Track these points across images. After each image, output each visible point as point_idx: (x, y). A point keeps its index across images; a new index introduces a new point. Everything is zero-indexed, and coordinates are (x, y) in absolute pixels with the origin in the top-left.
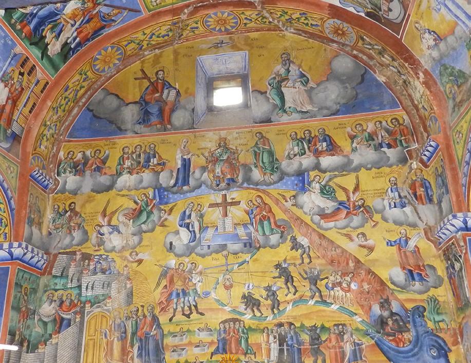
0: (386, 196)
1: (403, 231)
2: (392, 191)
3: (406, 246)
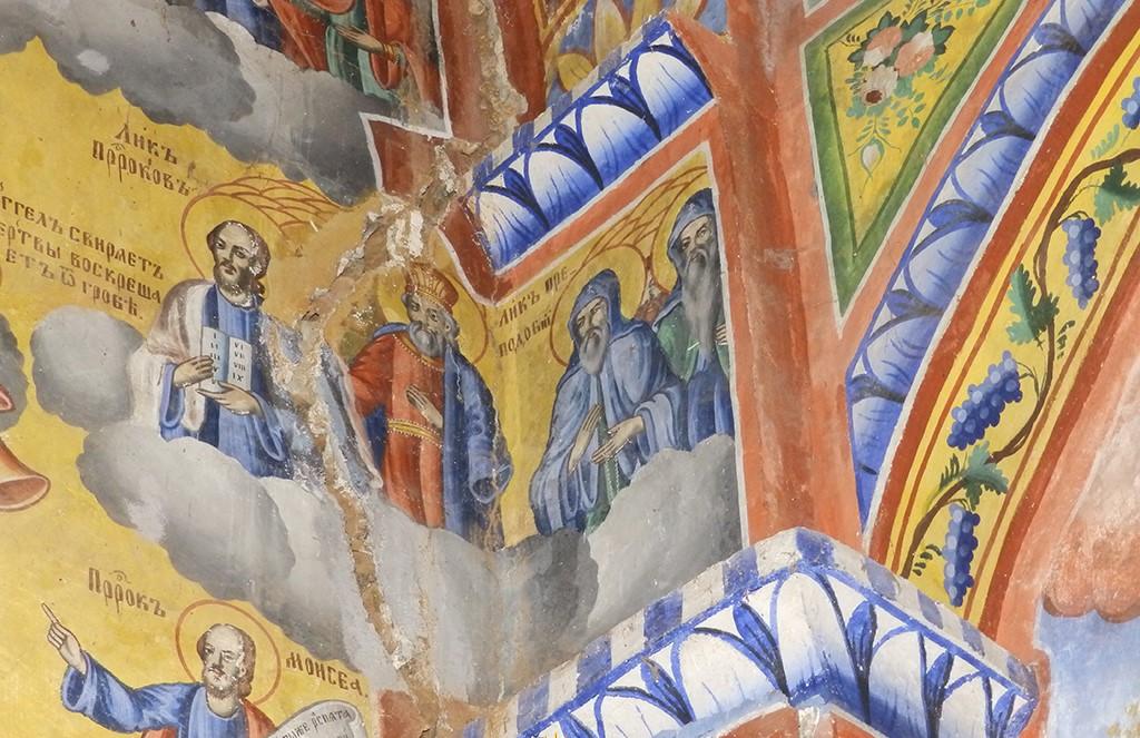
0: (163, 324)
1: (224, 641)
2: (212, 317)
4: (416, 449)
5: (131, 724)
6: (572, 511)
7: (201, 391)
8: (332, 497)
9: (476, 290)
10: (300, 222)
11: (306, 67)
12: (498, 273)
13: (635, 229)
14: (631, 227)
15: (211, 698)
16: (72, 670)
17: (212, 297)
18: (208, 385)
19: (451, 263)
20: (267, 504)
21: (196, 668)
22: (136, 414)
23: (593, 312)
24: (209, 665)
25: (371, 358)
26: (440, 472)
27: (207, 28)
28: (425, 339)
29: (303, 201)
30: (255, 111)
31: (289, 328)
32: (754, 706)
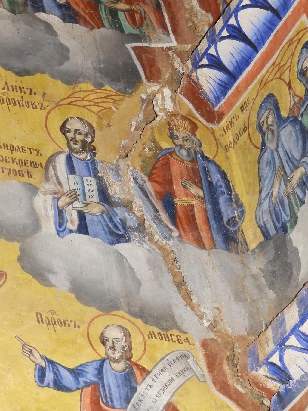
0: (47, 179)
1: (113, 334)
2: (71, 169)
3: (128, 400)
4: (192, 211)
5: (74, 387)
6: (279, 224)
7: (74, 208)
8: (154, 247)
9: (206, 121)
10: (106, 108)
11: (92, 28)
12: (216, 109)
13: (279, 70)
14: (276, 69)
15: (113, 364)
16: (38, 366)
17: (69, 159)
18: (77, 204)
19: (190, 109)
20: (120, 258)
21: (102, 350)
22: (43, 228)
23: (267, 118)
24: (108, 348)
25: (159, 169)
26: (208, 220)
27: (37, 22)
28: (184, 153)
29: (106, 97)
30: (71, 57)
31: (112, 164)
32: (255, 380)
